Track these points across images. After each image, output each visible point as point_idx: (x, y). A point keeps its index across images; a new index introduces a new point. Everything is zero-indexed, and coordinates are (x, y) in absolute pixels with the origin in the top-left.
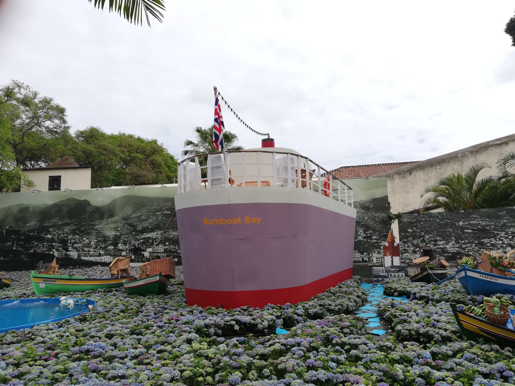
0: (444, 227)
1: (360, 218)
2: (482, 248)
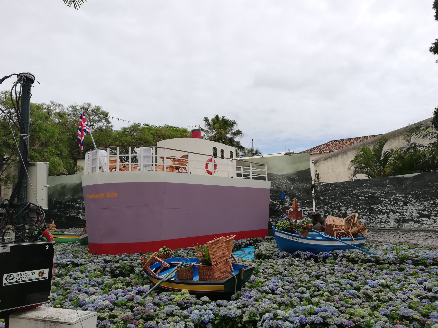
0: (345, 195)
1: (287, 188)
2: (372, 214)
